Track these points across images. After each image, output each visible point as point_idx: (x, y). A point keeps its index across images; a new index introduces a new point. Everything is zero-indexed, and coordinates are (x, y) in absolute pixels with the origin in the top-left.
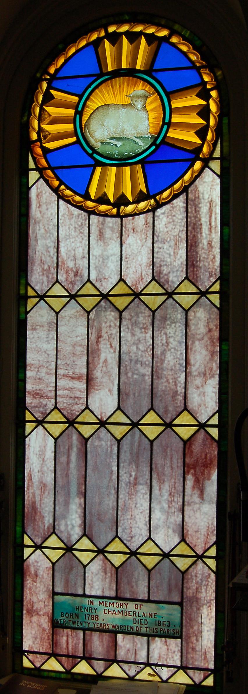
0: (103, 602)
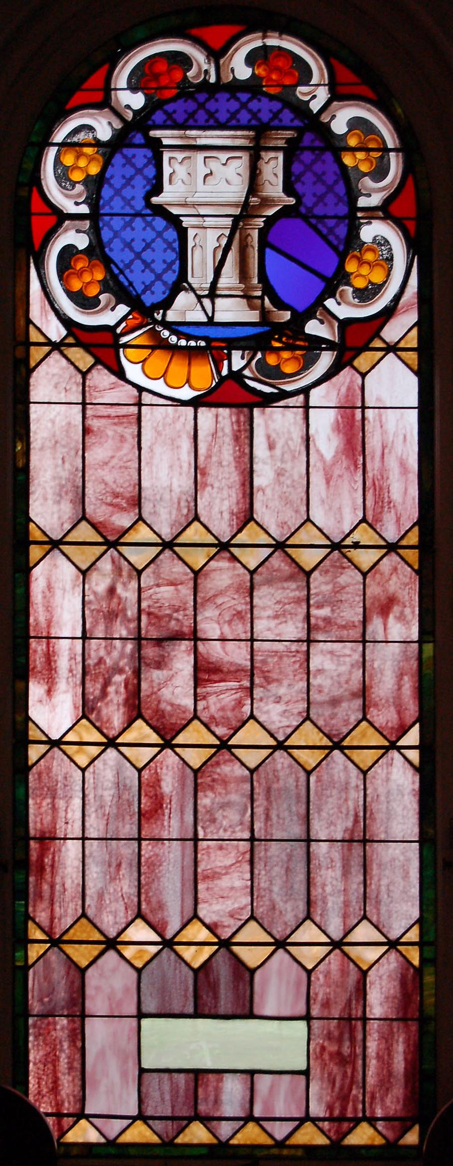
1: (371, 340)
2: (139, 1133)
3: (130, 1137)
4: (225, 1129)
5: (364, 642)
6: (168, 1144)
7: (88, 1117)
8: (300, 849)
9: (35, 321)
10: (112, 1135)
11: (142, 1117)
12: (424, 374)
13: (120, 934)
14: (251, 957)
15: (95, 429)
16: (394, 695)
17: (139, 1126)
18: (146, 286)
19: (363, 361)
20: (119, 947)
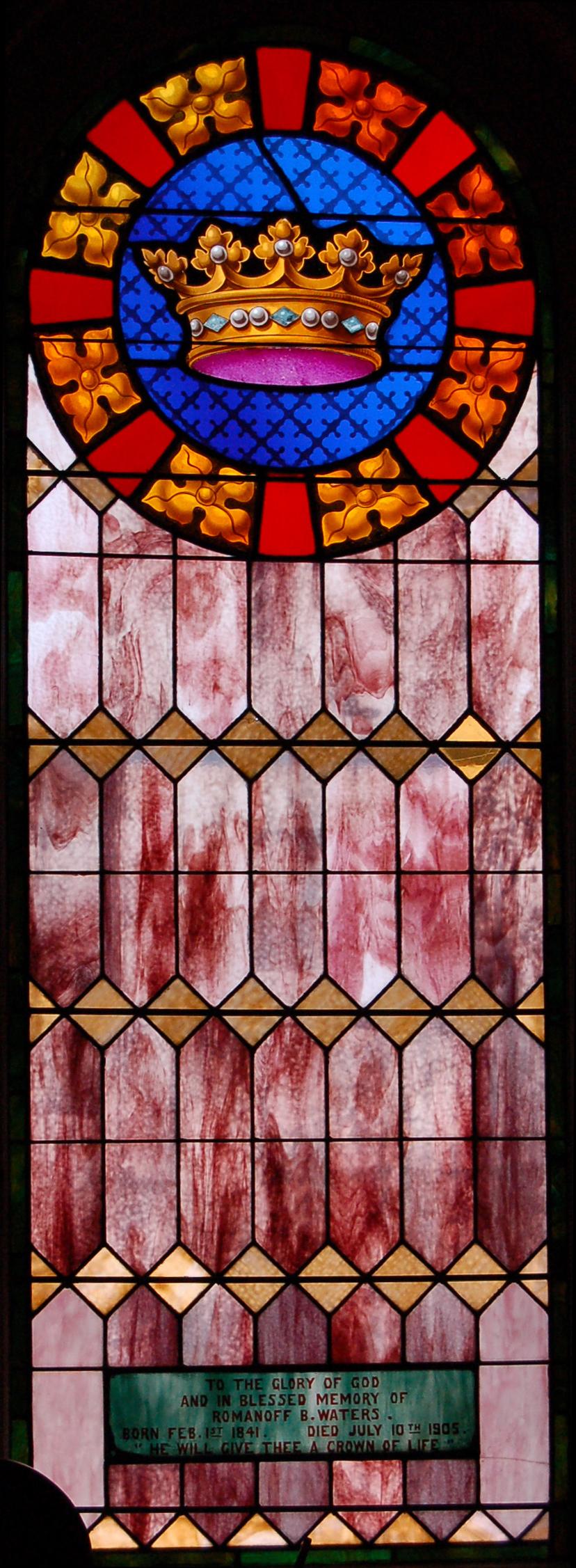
0: (326, 1396)
1: (479, 472)
2: (406, 1532)
3: (393, 1536)
4: (369, 1524)
5: (399, 872)
6: (220, 1547)
7: (484, 1508)
8: (392, 1148)
9: (431, 476)
10: (516, 1532)
11: (406, 1508)
12: (544, 516)
13: (154, 1267)
14: (179, 1296)
15: (345, 607)
16: (57, 931)
17: (405, 1522)
18: (193, 403)
19: (466, 502)
20: (77, 1285)
